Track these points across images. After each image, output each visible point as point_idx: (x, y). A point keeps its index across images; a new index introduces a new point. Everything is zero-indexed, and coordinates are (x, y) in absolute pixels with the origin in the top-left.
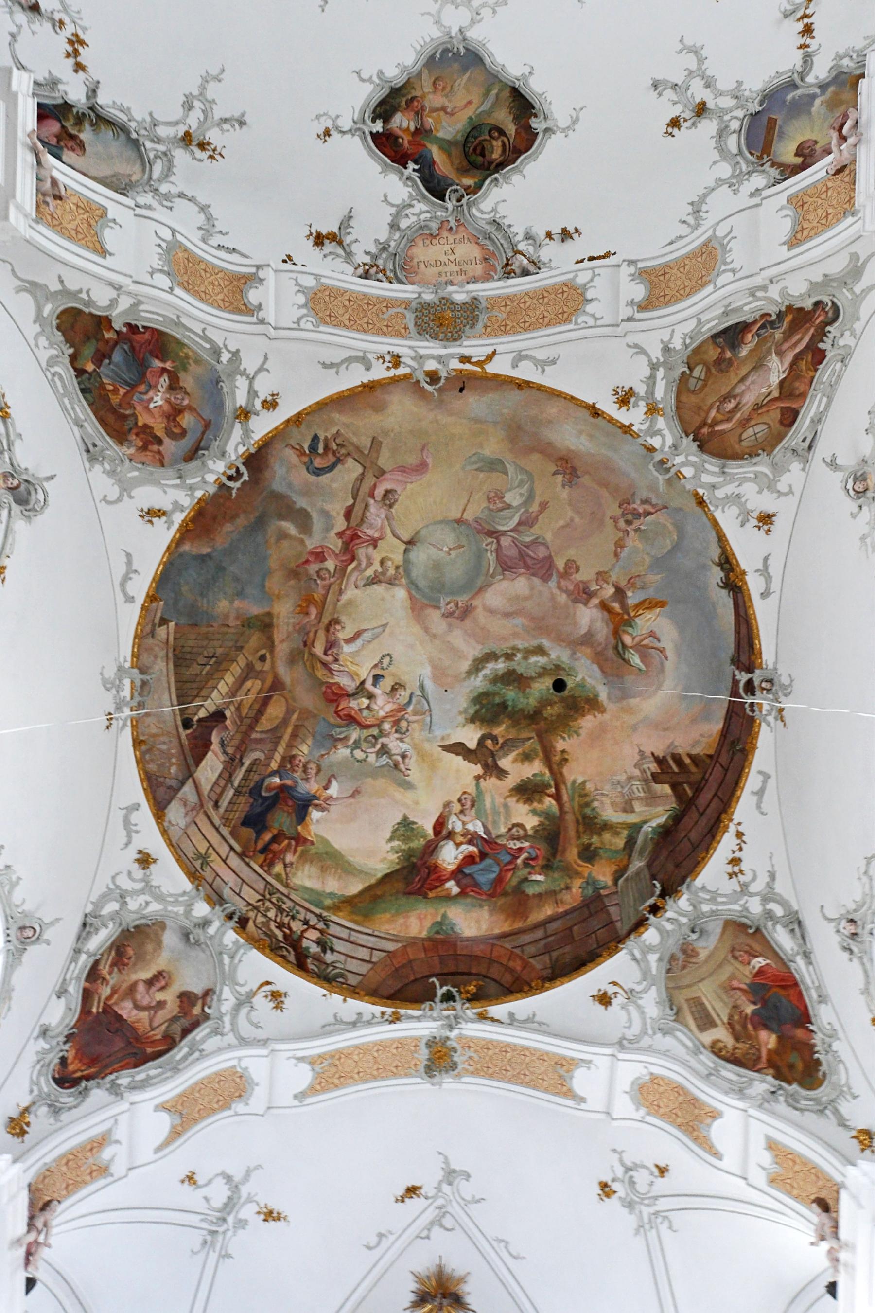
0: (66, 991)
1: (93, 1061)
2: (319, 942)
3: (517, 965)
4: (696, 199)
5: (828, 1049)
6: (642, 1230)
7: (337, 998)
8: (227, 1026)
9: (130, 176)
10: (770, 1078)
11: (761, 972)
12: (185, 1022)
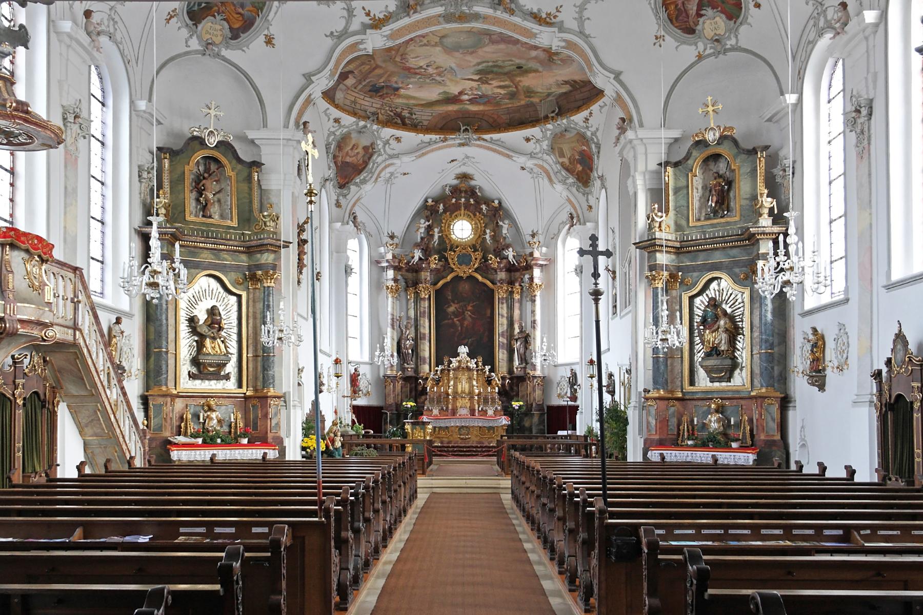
1: (346, 178)
3: (496, 117)
11: (584, 150)
12: (368, 155)
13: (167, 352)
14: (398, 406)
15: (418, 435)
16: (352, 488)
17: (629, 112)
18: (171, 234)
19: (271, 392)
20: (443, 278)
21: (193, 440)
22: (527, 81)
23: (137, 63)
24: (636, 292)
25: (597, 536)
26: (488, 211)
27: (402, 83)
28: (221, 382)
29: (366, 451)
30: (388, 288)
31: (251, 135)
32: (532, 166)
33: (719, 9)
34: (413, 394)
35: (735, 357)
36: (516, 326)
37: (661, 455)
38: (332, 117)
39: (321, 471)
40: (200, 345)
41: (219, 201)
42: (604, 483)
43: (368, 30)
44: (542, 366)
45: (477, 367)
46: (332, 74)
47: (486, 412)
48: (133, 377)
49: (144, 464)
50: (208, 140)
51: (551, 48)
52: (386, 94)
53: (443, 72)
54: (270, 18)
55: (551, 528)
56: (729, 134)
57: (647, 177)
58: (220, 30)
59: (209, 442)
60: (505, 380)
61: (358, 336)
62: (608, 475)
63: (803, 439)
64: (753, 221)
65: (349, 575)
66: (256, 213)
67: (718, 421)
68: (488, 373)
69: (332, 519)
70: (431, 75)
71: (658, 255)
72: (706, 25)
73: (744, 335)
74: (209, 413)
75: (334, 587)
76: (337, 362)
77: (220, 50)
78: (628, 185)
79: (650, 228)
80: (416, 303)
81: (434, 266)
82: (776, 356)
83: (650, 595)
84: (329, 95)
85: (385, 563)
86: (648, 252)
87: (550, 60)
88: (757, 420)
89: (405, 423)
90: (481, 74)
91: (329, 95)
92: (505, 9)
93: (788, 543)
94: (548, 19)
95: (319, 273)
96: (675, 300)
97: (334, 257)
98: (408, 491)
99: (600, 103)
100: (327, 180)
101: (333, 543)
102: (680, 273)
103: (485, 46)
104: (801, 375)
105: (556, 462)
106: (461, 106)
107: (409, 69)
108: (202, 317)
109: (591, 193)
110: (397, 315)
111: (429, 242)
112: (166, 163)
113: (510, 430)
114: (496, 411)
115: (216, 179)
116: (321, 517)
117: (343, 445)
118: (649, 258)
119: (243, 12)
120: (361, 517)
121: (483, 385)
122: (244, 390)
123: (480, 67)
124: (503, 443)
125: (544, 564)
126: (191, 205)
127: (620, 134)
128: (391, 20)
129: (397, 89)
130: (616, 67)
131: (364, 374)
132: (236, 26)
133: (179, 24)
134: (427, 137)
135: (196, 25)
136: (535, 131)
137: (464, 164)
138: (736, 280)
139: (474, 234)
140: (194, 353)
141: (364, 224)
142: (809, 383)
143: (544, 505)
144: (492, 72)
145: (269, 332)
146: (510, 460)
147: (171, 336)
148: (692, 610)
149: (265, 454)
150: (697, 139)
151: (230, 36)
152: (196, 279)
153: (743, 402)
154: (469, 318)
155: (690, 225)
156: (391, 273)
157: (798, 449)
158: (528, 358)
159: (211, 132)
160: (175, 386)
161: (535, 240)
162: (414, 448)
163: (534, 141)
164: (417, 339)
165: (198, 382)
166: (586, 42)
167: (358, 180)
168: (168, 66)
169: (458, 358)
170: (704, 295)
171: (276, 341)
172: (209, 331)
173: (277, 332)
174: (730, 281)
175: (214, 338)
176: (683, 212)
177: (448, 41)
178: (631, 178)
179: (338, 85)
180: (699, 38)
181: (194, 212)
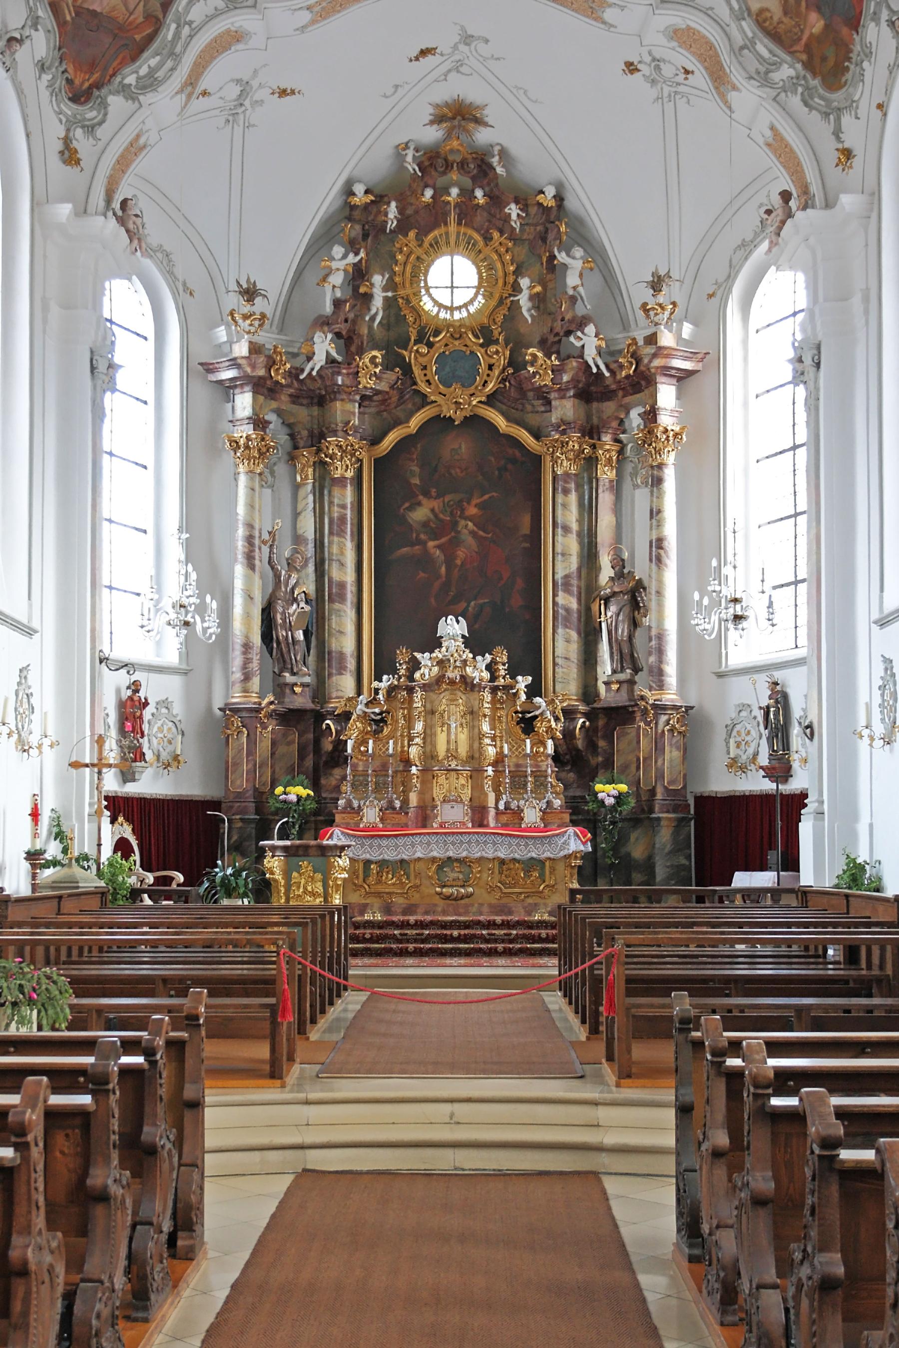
0: (38, 17)
5: (859, 64)
6: (660, 101)
10: (799, 66)
14: (261, 798)
30: (235, 444)
34: (309, 762)
45: (493, 678)
47: (518, 814)
68: (523, 697)
81: (371, 383)
110: (264, 525)
111: (359, 317)
114: (546, 813)
131: (165, 704)
137: (457, 68)
139: (488, 296)
154: (470, 541)
156: (244, 403)
158: (640, 654)
161: (661, 299)
167: (131, 80)
169: (437, 654)
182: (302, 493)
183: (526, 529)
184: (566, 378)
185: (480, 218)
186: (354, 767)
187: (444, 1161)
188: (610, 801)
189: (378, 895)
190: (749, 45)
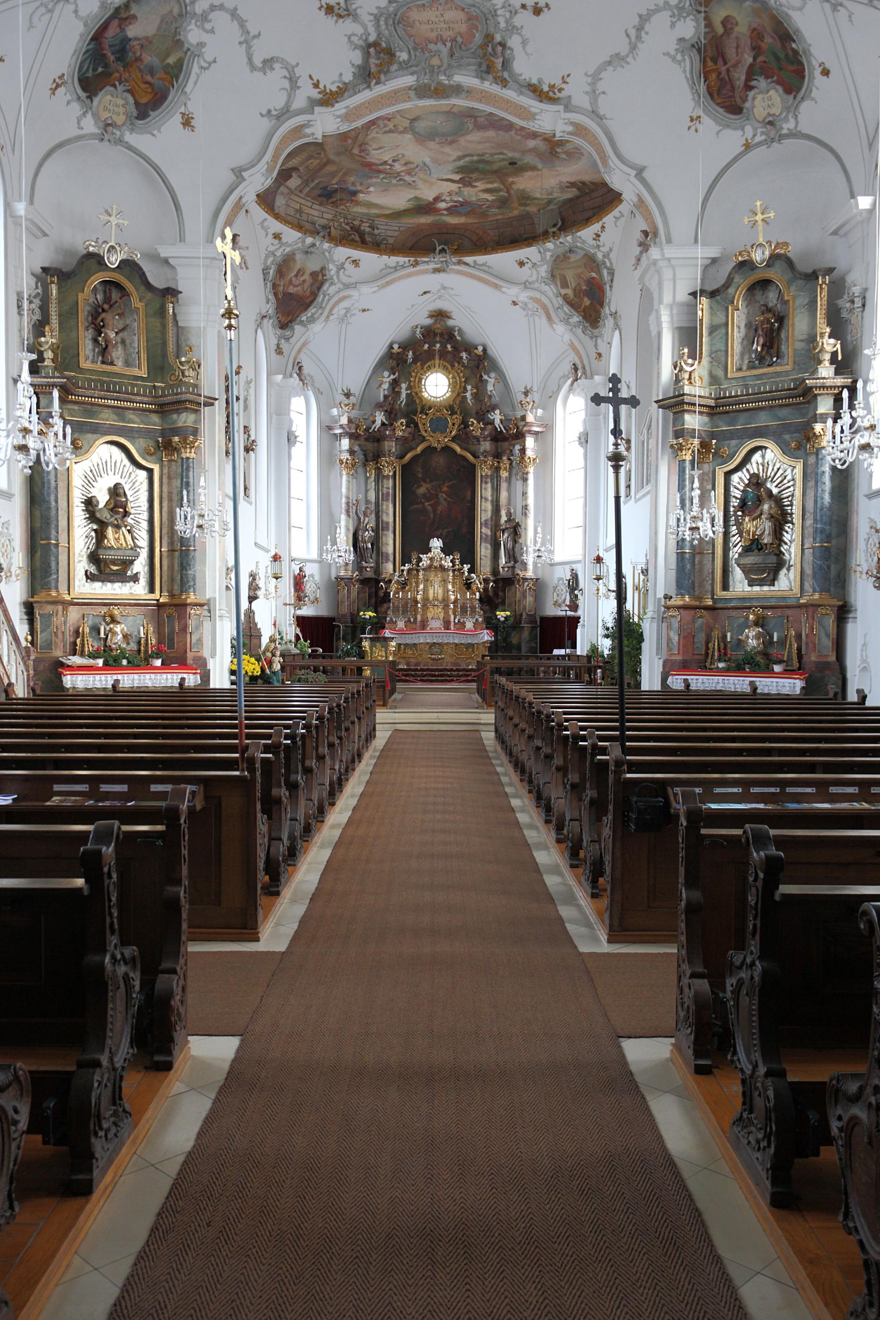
1: (288, 315)
2: (369, 227)
3: (481, 233)
4: (645, 12)
7: (385, 257)
8: (336, 281)
9: (171, 12)
11: (593, 278)
12: (317, 284)
13: (57, 545)
15: (380, 654)
16: (287, 727)
17: (654, 223)
18: (60, 386)
19: (192, 598)
20: (412, 449)
21: (91, 662)
22: (524, 183)
23: (13, 150)
24: (657, 467)
25: (611, 796)
26: (469, 360)
27: (361, 184)
28: (128, 584)
29: (312, 676)
30: (341, 462)
31: (164, 252)
32: (526, 300)
33: (775, 78)
34: (373, 601)
35: (781, 552)
36: (503, 513)
37: (686, 681)
38: (271, 232)
39: (244, 703)
40: (100, 535)
41: (123, 342)
42: (622, 721)
43: (316, 108)
44: (535, 564)
45: (453, 566)
46: (270, 170)
48: (14, 578)
49: (28, 693)
50: (108, 258)
51: (554, 135)
52: (341, 200)
53: (414, 169)
54: (188, 89)
55: (547, 780)
56: (782, 252)
57: (675, 312)
58: (123, 106)
59: (112, 663)
60: (489, 584)
61: (304, 525)
62: (628, 708)
63: (864, 661)
64: (811, 370)
65: (282, 848)
66: (171, 358)
67: (757, 637)
68: (466, 574)
69: (258, 773)
70: (398, 173)
71: (687, 417)
72: (756, 102)
73: (793, 524)
74: (112, 626)
75: (261, 865)
76: (276, 558)
77: (122, 135)
78: (650, 322)
79: (677, 380)
80: (377, 481)
82: (833, 551)
83: (688, 885)
84: (266, 200)
85: (333, 827)
86: (675, 413)
87: (551, 153)
88: (807, 635)
89: (361, 639)
90: (463, 173)
91: (266, 200)
92: (495, 78)
93: (866, 805)
94: (551, 94)
95: (254, 441)
96: (706, 478)
97: (274, 420)
98: (364, 728)
99: (615, 213)
100: (265, 317)
101: (259, 806)
102: (714, 441)
103: (469, 132)
104: (864, 576)
105: (551, 690)
106: (437, 218)
107: (369, 165)
108: (103, 498)
109: (601, 335)
110: (353, 498)
112: (54, 289)
113: (494, 648)
114: (476, 624)
115: (120, 311)
116: (243, 770)
117: (283, 668)
118: (675, 420)
119: (152, 81)
120: (300, 767)
121: (460, 589)
122: (157, 595)
123: (461, 163)
124: (485, 665)
125: (537, 828)
126: (86, 347)
127: (641, 252)
128: (346, 94)
129: (355, 193)
130: (639, 161)
131: (312, 576)
132: (144, 100)
133: (69, 97)
134: (394, 260)
135: (90, 97)
136: (530, 252)
137: (440, 298)
138: (786, 450)
139: (452, 391)
140: (92, 547)
141: (311, 377)
142: (875, 587)
143: (538, 749)
144: (477, 169)
145: (186, 518)
146: (493, 688)
147: (63, 523)
148: (756, 915)
149: (183, 679)
150: (740, 259)
151: (135, 114)
152: (94, 446)
153: (789, 612)
154: (445, 503)
155: (729, 376)
156: (345, 443)
157: (857, 673)
158: (518, 555)
159: (112, 247)
160: (69, 590)
162: (372, 673)
163: (530, 265)
164: (378, 530)
165: (97, 585)
166: (600, 126)
167: (304, 318)
168: (55, 155)
169: (429, 555)
170: (744, 470)
171: (195, 529)
172: (112, 516)
173: (196, 517)
174: (777, 451)
175: (118, 527)
176: (719, 358)
177: (420, 126)
178: (654, 313)
179: (279, 188)
180: (748, 119)
181: (91, 357)
182: (369, 481)
183: (469, 498)
184: (486, 433)
185: (449, 357)
186: (393, 603)
187: (436, 727)
188: (502, 619)
189: (404, 658)
190: (560, 307)
